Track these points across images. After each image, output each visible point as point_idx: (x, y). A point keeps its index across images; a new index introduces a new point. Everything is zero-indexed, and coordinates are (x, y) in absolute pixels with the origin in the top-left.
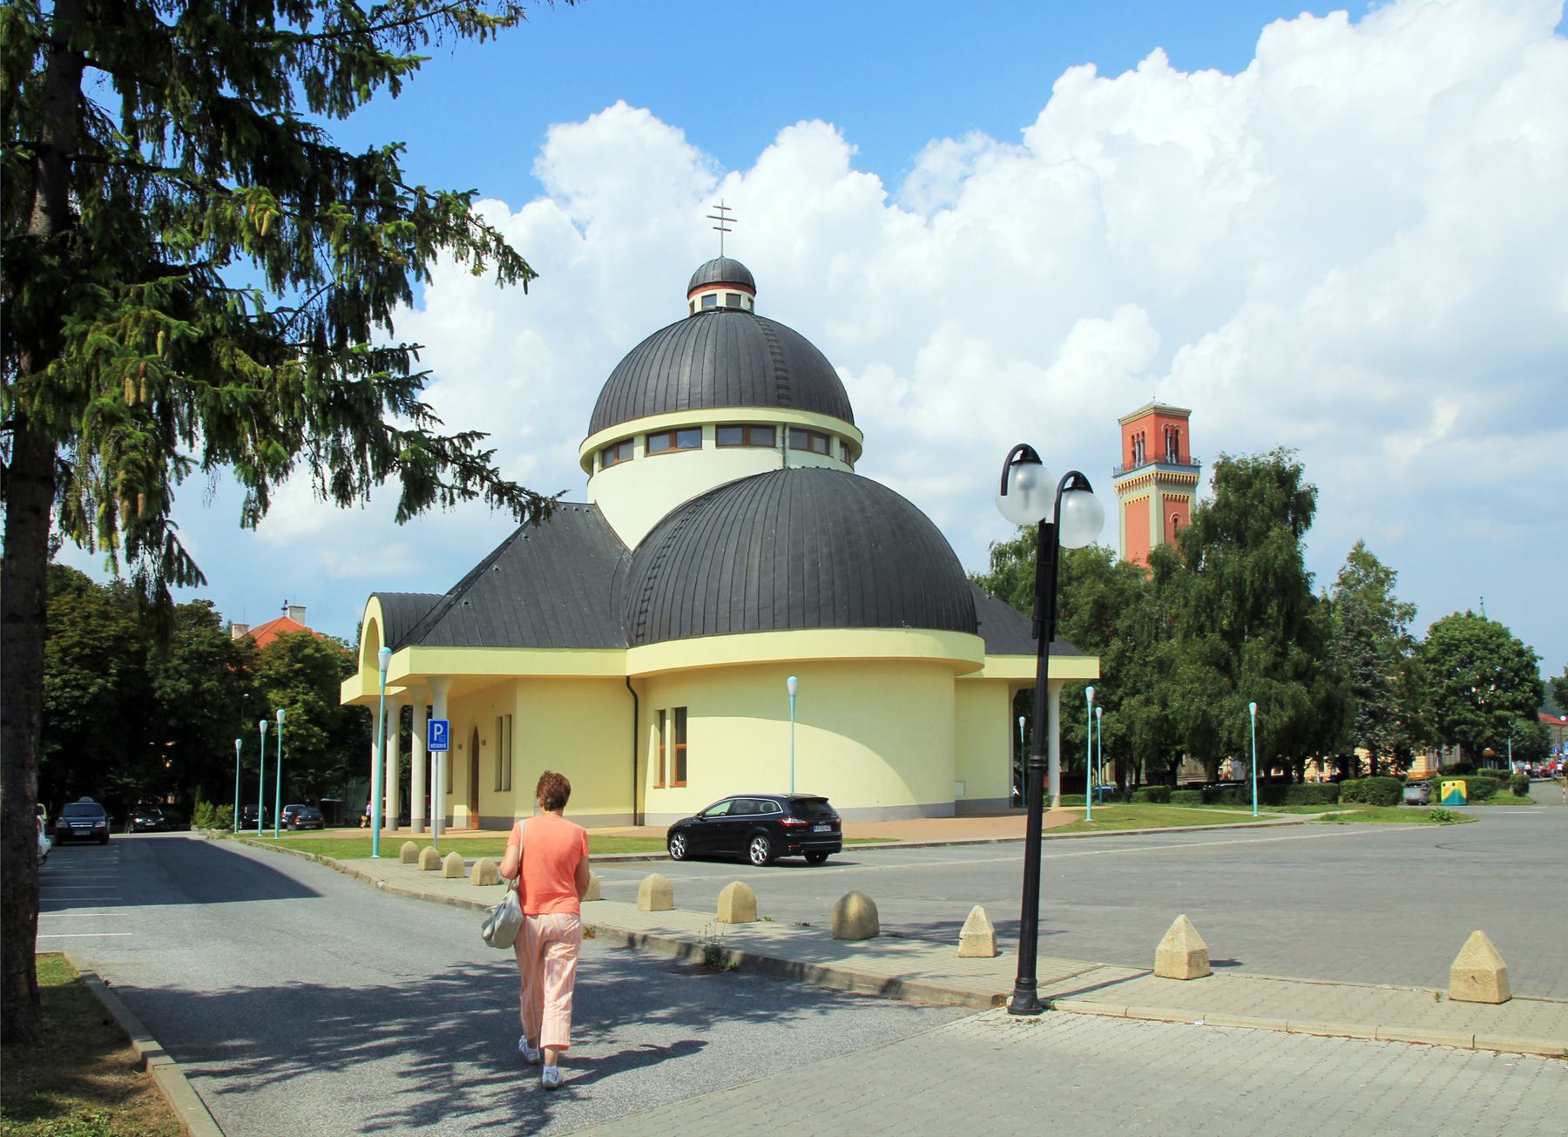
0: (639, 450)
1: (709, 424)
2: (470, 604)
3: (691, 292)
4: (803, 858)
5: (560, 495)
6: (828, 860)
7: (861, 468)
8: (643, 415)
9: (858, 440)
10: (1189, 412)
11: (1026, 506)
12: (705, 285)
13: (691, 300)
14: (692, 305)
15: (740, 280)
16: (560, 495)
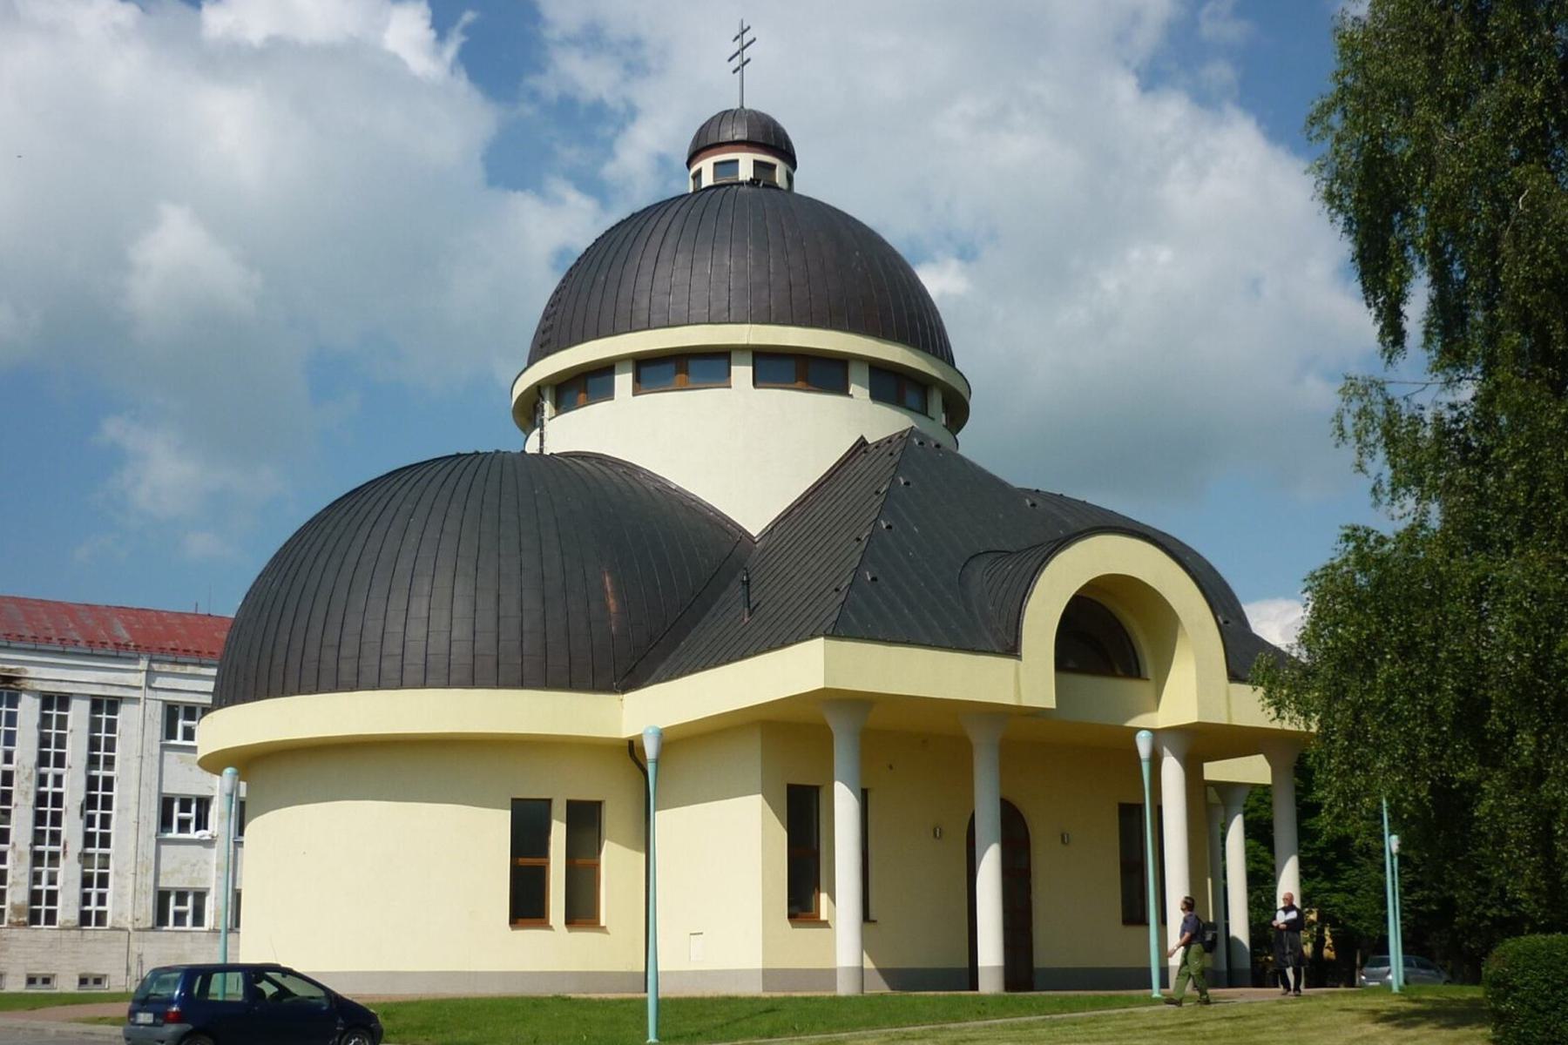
0: (623, 381)
1: (622, 359)
2: (881, 580)
3: (694, 156)
5: (541, 436)
8: (649, 326)
9: (967, 398)
10: (862, 437)
11: (1341, 527)
13: (694, 169)
14: (697, 176)
16: (541, 436)
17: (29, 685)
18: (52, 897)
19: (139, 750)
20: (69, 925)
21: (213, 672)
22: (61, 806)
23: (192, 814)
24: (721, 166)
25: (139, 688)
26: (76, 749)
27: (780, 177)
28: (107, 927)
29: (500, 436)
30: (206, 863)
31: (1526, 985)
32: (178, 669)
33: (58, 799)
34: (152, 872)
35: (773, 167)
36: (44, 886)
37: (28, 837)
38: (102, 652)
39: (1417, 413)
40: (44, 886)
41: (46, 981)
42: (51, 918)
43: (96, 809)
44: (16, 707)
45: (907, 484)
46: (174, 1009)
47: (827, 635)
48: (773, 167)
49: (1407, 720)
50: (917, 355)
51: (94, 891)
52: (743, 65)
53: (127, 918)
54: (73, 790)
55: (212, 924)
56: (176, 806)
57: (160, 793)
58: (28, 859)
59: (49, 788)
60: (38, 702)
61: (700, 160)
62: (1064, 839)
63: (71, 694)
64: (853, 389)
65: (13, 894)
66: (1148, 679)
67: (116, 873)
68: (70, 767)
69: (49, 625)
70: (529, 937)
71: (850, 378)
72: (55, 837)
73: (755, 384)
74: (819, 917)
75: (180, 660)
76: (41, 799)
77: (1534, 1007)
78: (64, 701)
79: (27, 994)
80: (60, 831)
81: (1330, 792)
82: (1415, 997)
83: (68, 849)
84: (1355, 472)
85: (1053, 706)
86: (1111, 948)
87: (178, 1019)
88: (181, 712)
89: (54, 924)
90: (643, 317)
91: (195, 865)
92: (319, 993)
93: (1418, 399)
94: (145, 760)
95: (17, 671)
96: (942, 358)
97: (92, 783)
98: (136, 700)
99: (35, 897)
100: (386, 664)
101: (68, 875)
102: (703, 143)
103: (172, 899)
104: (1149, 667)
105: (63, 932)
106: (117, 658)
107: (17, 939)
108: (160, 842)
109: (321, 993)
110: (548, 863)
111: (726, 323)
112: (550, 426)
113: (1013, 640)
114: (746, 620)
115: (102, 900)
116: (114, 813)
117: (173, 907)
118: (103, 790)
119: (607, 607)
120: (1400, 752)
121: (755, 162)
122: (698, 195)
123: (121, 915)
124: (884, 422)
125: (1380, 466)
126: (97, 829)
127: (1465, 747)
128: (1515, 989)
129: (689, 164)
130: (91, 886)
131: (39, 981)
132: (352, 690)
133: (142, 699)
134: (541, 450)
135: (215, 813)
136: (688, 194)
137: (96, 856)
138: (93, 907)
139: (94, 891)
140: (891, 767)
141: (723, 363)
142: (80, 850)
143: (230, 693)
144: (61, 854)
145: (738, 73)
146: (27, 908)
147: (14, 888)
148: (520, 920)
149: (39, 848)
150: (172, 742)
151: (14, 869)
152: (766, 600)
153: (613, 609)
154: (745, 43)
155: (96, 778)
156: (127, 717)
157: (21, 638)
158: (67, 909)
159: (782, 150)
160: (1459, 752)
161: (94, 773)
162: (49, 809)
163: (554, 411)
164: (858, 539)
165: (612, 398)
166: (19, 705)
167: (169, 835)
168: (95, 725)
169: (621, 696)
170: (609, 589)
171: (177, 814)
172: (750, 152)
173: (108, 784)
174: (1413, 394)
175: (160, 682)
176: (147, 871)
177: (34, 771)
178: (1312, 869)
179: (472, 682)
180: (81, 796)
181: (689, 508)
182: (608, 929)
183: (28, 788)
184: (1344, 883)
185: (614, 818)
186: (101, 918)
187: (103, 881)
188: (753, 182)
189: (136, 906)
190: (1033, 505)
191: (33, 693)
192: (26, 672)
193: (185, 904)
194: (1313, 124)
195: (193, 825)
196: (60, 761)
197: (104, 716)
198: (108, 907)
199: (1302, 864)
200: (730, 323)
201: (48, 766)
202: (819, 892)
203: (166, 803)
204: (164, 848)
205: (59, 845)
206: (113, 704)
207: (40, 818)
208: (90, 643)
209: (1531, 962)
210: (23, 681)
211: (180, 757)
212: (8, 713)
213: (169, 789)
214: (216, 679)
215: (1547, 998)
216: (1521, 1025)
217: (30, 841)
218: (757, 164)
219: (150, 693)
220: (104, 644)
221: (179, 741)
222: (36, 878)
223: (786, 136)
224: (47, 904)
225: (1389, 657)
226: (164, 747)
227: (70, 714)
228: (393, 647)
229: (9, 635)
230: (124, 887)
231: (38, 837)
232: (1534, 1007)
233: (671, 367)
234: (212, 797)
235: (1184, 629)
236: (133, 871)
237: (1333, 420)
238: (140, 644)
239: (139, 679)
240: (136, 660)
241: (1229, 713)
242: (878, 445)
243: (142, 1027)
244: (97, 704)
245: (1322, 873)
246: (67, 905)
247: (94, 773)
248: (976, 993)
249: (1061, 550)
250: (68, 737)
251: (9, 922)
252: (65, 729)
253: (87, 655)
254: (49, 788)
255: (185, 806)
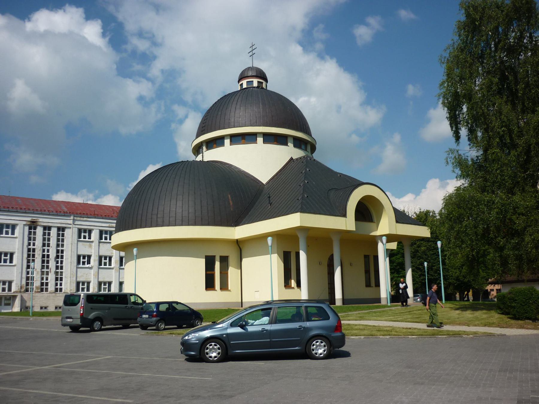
0: (227, 141)
3: (240, 79)
4: (176, 326)
5: (203, 156)
6: (148, 329)
7: (316, 156)
9: (315, 144)
10: (292, 157)
12: (248, 77)
14: (242, 85)
15: (261, 75)
16: (203, 156)
17: (40, 224)
18: (47, 284)
19: (71, 242)
20: (52, 292)
21: (115, 221)
22: (49, 258)
23: (86, 260)
24: (249, 82)
25: (71, 224)
26: (53, 242)
27: (264, 86)
28: (63, 292)
29: (191, 157)
30: (90, 274)
31: (519, 299)
32: (82, 219)
33: (48, 256)
34: (75, 277)
35: (262, 83)
36: (44, 281)
37: (40, 267)
38: (60, 214)
39: (466, 158)
40: (44, 281)
41: (46, 308)
42: (47, 290)
43: (59, 259)
44: (36, 230)
45: (309, 170)
46: (155, 314)
47: (301, 212)
48: (262, 83)
49: (470, 235)
50: (305, 135)
51: (59, 282)
52: (253, 55)
53: (68, 290)
54: (53, 254)
55: (92, 291)
56: (82, 258)
57: (77, 254)
58: (40, 273)
59: (46, 253)
60: (42, 228)
61: (242, 81)
62: (351, 265)
63: (52, 226)
64: (289, 144)
65: (36, 283)
66: (375, 222)
67: (65, 277)
68: (51, 247)
69: (44, 206)
70: (211, 293)
71: (288, 142)
72: (48, 267)
73: (264, 143)
74: (291, 286)
75: (82, 216)
76: (43, 256)
77: (521, 304)
78: (49, 228)
79: (55, 312)
80: (49, 265)
81: (448, 253)
82: (454, 304)
83: (51, 270)
84: (452, 173)
85: (355, 230)
86: (368, 293)
87: (156, 316)
88: (83, 231)
89: (48, 292)
90: (232, 124)
91: (87, 274)
92: (187, 308)
93: (466, 155)
94: (73, 245)
95: (36, 220)
96: (310, 136)
97: (58, 251)
98: (70, 228)
99: (42, 284)
100: (171, 219)
101: (51, 277)
102: (243, 76)
103: (81, 284)
104: (375, 219)
105: (50, 294)
106: (64, 216)
107: (37, 296)
108: (77, 268)
109: (189, 308)
110: (215, 273)
111: (255, 126)
112: (205, 153)
113: (344, 212)
114: (269, 207)
115: (61, 285)
116: (64, 260)
117: (81, 286)
118: (61, 253)
119: (229, 204)
120: (469, 243)
121: (258, 81)
122: (241, 91)
123: (67, 289)
124: (297, 153)
125: (458, 171)
126: (59, 264)
127: (484, 242)
128: (516, 300)
129: (239, 82)
130: (58, 281)
131: (44, 308)
132: (162, 226)
133: (72, 227)
134: (203, 160)
135: (92, 259)
136: (239, 91)
137: (59, 272)
138: (59, 287)
139: (59, 282)
140: (308, 246)
141: (254, 137)
142: (55, 271)
143: (121, 227)
144: (49, 271)
145: (251, 57)
146: (40, 287)
147: (36, 282)
148: (208, 288)
149: (43, 270)
150: (80, 239)
151: (36, 276)
152: (274, 202)
153: (231, 204)
154: (253, 49)
155: (59, 250)
156: (67, 232)
157: (37, 210)
158: (51, 287)
159: (265, 78)
160: (483, 243)
161: (58, 248)
162: (46, 259)
163: (206, 149)
164: (300, 186)
165: (224, 146)
166: (37, 229)
167: (80, 266)
168: (58, 235)
169: (234, 228)
170: (230, 199)
171: (82, 260)
172: (257, 79)
173: (62, 251)
174: (465, 153)
175: (76, 223)
176: (74, 276)
177: (42, 248)
178: (393, 271)
179: (195, 224)
180: (55, 255)
181: (247, 177)
182: (231, 290)
183: (40, 253)
184: (401, 275)
185: (232, 260)
186: (61, 290)
187: (61, 279)
188: (258, 87)
189: (71, 286)
190: (340, 176)
191: (41, 226)
192: (39, 220)
193: (84, 285)
194: (441, 86)
195: (86, 263)
196: (49, 245)
197: (61, 232)
198: (63, 287)
199: (413, 271)
200: (256, 126)
201: (45, 247)
202: (291, 279)
203: (79, 257)
204: (78, 270)
205: (49, 269)
206: (63, 229)
207: (43, 262)
208: (57, 212)
209: (520, 294)
210: (38, 223)
211: (83, 244)
212: (48, 232)
213: (79, 253)
214: (116, 223)
215: (524, 302)
216: (518, 309)
217: (40, 268)
218: (258, 82)
219: (74, 226)
220: (45, 210)
221: (103, 240)
222: (42, 279)
223: (265, 74)
224: (46, 286)
225: (466, 219)
226: (78, 241)
227: (52, 232)
228: (173, 214)
229: (33, 209)
230: (67, 281)
231: (43, 267)
232: (521, 304)
233: (240, 138)
234: (91, 255)
235: (385, 211)
236: (70, 276)
237: (445, 159)
238: (70, 212)
239: (71, 222)
240: (70, 216)
241: (346, 226)
242: (297, 159)
243: (145, 319)
244: (59, 229)
245: (396, 272)
246: (51, 286)
247: (58, 248)
248: (335, 305)
249: (356, 189)
250: (65, 239)
251: (35, 291)
252: (50, 236)
253: (56, 215)
254: (46, 253)
255: (84, 258)
